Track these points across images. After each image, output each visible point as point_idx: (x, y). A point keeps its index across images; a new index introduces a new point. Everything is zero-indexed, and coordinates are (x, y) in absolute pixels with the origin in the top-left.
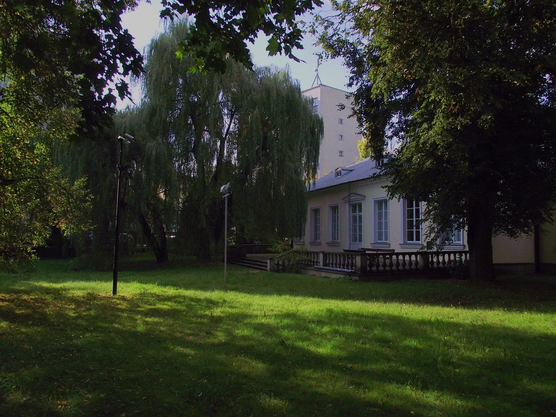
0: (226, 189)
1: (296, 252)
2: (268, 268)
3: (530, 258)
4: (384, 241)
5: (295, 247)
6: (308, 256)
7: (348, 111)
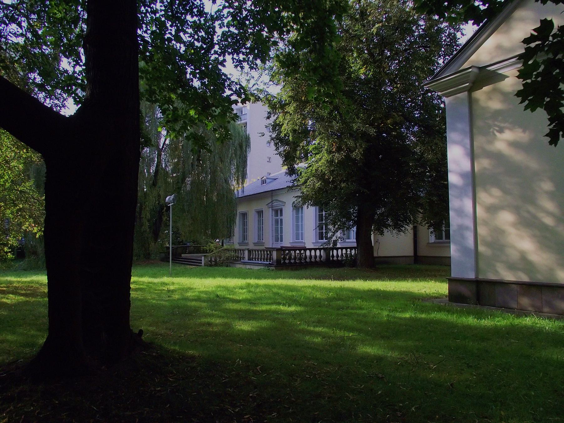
0: (171, 199)
1: (226, 250)
2: (203, 264)
3: (409, 252)
4: (300, 240)
5: (225, 247)
6: (236, 253)
7: (267, 138)
